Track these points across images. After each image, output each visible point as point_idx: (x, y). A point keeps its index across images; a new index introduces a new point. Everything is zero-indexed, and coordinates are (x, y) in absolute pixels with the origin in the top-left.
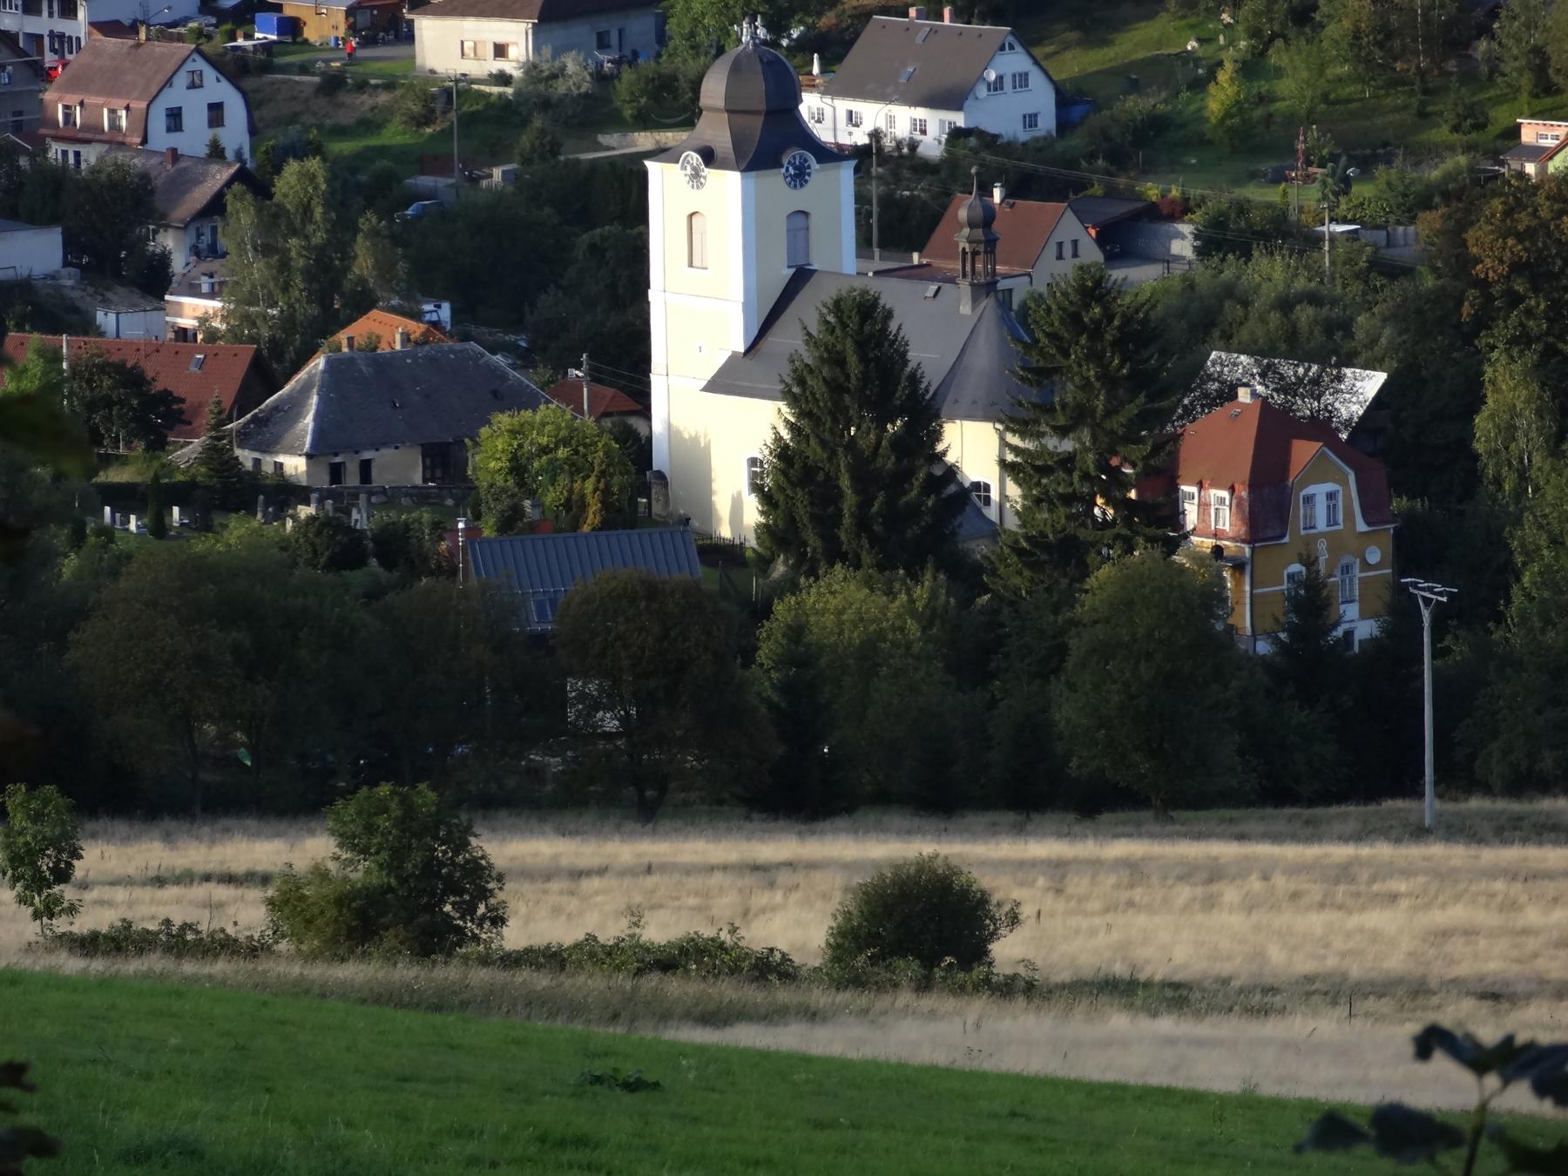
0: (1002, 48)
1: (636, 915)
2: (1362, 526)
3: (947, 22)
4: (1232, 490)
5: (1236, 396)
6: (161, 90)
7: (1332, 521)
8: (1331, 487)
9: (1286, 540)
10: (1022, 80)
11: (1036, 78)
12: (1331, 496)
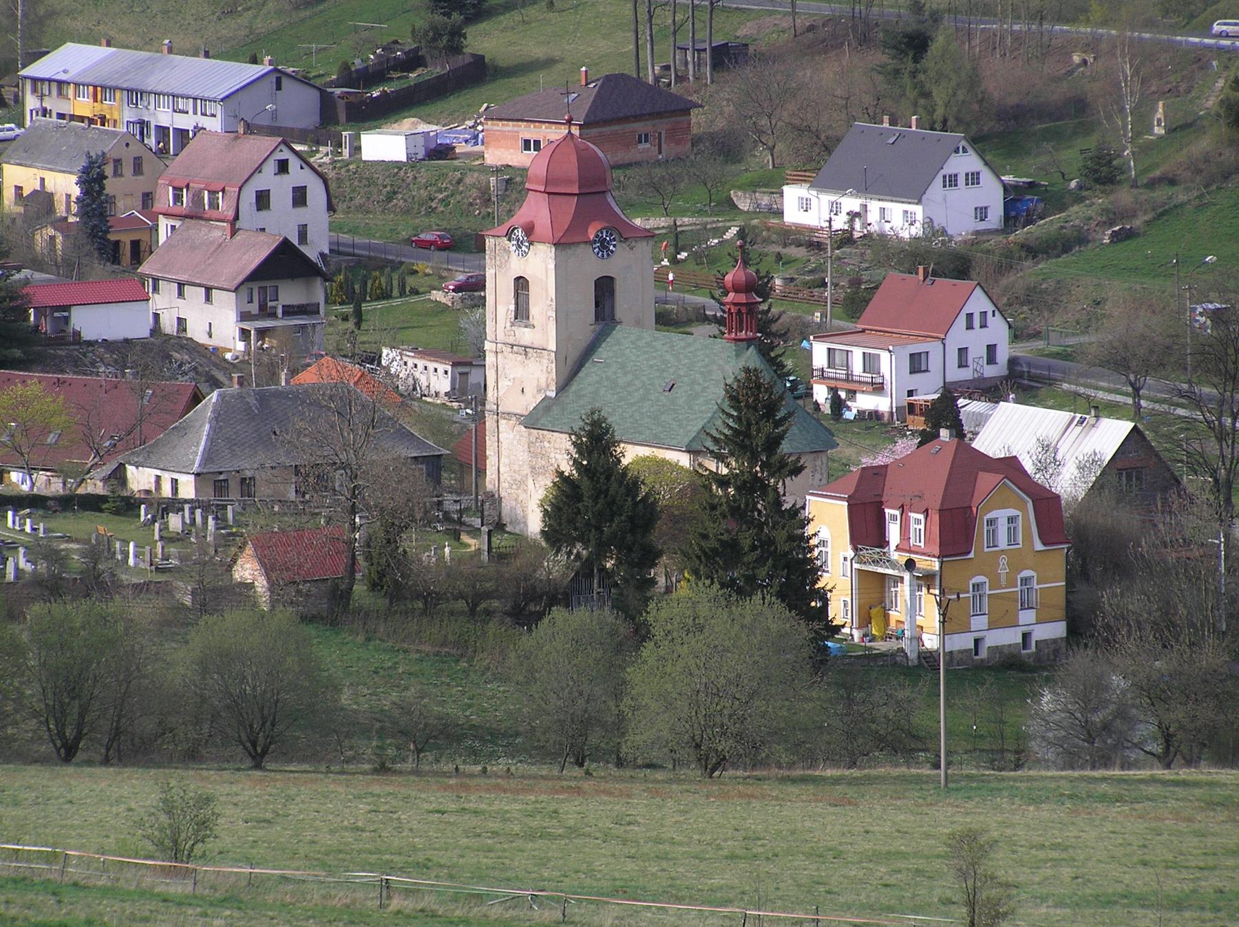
0: (957, 151)
1: (179, 843)
2: (1039, 546)
3: (914, 129)
4: (926, 512)
5: (938, 436)
6: (252, 175)
7: (1012, 539)
8: (1012, 512)
9: (972, 555)
10: (973, 179)
11: (987, 176)
12: (1011, 520)
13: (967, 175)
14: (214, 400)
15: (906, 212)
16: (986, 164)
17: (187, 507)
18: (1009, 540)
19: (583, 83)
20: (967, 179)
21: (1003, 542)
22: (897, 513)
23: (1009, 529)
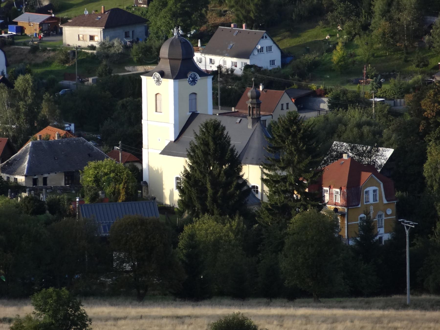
0: (263, 38)
2: (385, 202)
3: (244, 29)
4: (341, 189)
5: (342, 157)
7: (375, 200)
8: (375, 188)
9: (360, 206)
10: (269, 49)
11: (274, 48)
12: (375, 191)
13: (267, 47)
14: (30, 145)
15: (211, 59)
16: (274, 43)
17: (28, 189)
18: (374, 200)
19: (103, 12)
20: (267, 49)
21: (371, 201)
22: (328, 189)
23: (374, 195)
